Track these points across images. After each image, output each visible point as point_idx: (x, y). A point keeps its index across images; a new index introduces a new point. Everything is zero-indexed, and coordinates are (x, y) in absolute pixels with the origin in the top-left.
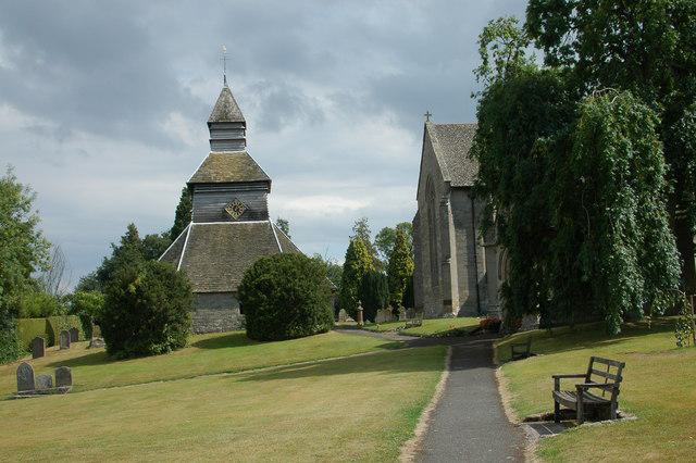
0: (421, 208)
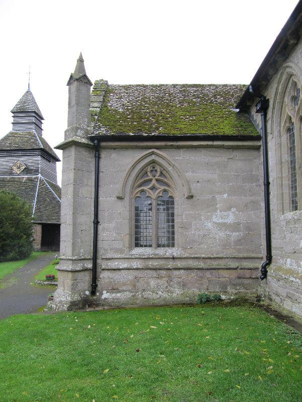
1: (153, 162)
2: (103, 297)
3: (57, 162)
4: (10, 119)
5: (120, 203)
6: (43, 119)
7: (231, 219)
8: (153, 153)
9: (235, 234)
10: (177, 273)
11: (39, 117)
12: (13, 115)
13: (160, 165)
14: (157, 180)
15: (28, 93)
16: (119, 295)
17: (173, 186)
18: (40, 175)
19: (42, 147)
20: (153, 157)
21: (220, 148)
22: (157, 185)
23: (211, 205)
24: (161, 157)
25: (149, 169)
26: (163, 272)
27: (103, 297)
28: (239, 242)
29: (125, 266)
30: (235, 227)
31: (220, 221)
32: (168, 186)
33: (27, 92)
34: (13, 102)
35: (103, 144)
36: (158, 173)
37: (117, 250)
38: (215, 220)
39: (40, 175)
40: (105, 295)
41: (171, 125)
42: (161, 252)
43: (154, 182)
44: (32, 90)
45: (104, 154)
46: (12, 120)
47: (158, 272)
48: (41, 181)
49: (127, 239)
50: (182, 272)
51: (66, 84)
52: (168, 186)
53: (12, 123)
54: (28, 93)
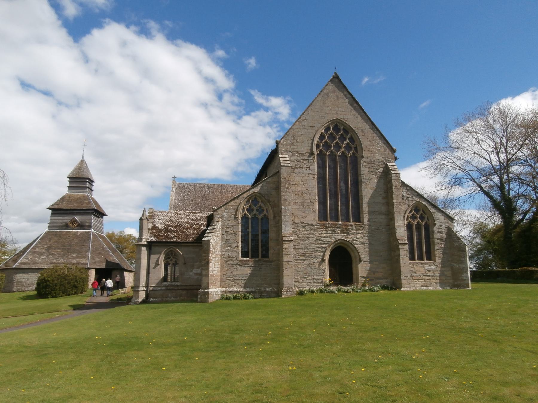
1: (171, 251)
2: (151, 300)
3: (104, 217)
4: (66, 182)
6: (93, 182)
8: (171, 248)
12: (69, 179)
14: (173, 257)
15: (83, 162)
16: (157, 299)
18: (92, 230)
19: (96, 208)
20: (172, 249)
22: (173, 259)
23: (193, 267)
24: (173, 248)
25: (170, 253)
27: (151, 300)
29: (159, 289)
31: (196, 272)
33: (82, 161)
34: (69, 170)
35: (153, 244)
36: (173, 255)
37: (232, 219)
38: (194, 272)
39: (92, 230)
40: (152, 299)
43: (172, 258)
45: (153, 248)
46: (68, 184)
48: (94, 235)
50: (181, 291)
52: (177, 259)
53: (68, 186)
54: (83, 162)
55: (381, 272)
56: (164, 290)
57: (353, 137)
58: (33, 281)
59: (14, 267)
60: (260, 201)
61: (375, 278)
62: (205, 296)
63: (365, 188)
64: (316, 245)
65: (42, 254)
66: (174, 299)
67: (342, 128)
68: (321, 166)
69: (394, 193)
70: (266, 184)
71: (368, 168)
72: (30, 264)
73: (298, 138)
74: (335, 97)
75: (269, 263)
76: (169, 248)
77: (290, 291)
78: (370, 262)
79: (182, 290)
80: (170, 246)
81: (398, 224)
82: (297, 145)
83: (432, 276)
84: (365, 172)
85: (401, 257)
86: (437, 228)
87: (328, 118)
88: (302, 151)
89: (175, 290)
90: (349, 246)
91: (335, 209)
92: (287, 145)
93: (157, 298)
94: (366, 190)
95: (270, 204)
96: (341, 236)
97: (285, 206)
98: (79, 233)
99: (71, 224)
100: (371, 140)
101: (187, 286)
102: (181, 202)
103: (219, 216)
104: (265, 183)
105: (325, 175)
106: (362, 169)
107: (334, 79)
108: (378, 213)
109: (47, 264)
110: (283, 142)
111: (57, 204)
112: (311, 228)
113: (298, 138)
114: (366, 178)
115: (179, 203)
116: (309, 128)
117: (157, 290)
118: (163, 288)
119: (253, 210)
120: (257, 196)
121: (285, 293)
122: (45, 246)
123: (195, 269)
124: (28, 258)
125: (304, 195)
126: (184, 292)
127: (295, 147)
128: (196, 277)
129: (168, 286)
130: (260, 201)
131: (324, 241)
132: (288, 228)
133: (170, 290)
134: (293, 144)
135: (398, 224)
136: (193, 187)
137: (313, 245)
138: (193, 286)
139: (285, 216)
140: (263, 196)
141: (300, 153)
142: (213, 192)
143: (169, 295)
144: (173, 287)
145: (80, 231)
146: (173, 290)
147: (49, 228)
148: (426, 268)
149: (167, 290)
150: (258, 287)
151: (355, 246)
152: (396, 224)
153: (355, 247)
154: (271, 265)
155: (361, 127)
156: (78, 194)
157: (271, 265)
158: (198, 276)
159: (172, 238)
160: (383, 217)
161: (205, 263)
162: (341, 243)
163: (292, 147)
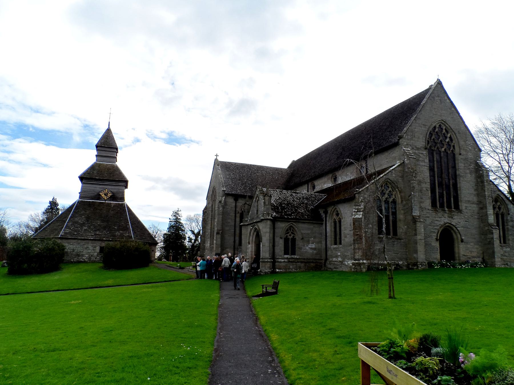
0: (208, 203)
1: (291, 226)
5: (281, 240)
7: (313, 246)
9: (315, 251)
10: (298, 263)
11: (115, 149)
13: (294, 228)
15: (109, 131)
17: (296, 234)
21: (12, 186)
23: (308, 242)
26: (294, 263)
28: (316, 254)
30: (315, 249)
31: (311, 247)
32: (295, 234)
38: (309, 246)
40: (277, 270)
41: (409, 176)
42: (293, 256)
43: (290, 233)
44: (111, 127)
47: (293, 263)
49: (283, 252)
50: (300, 263)
51: (225, 158)
52: (295, 234)
54: (109, 131)
55: (476, 252)
56: (287, 262)
57: (452, 136)
58: (78, 253)
59: (59, 236)
60: (390, 186)
61: (472, 256)
62: (361, 267)
63: (462, 181)
64: (431, 227)
65: (83, 225)
66: (295, 270)
67: (444, 128)
68: (431, 161)
69: (486, 186)
70: (395, 172)
71: (464, 164)
72: (74, 234)
73: (416, 134)
74: (439, 101)
75: (399, 241)
76: (289, 225)
77: (424, 265)
78: (8, 266)
79: (302, 262)
80: (291, 222)
81: (489, 213)
82: (414, 140)
83: (508, 256)
84: (462, 168)
85: (495, 240)
86: (510, 218)
87: (435, 119)
88: (418, 146)
89: (296, 262)
90: (453, 229)
91: (441, 196)
92: (408, 140)
93: (281, 269)
94: (463, 182)
95: (398, 190)
96: (447, 220)
97: (414, 192)
98: (113, 205)
99: (104, 195)
100: (465, 141)
101: (304, 259)
102: (230, 180)
103: (362, 198)
104: (394, 171)
105: (434, 166)
106: (460, 164)
107: (438, 85)
108: (472, 202)
109: (92, 235)
110: (405, 137)
111: (88, 173)
112: (427, 212)
113: (416, 134)
114: (462, 172)
115: (228, 181)
116: (422, 126)
117: (281, 262)
118: (286, 260)
119: (384, 194)
120: (389, 183)
121: (420, 266)
122: (83, 217)
123: (310, 244)
124: (70, 228)
125: (422, 184)
126: (303, 265)
127: (414, 142)
128: (311, 251)
129: (290, 259)
130: (390, 186)
131: (436, 224)
132: (417, 211)
133: (292, 262)
134: (411, 139)
135: (489, 213)
136: (235, 167)
137: (429, 227)
138: (309, 259)
139: (414, 201)
140: (393, 182)
141: (417, 147)
142: (255, 173)
143: (291, 267)
144: (294, 260)
145: (113, 203)
146: (294, 262)
147: (80, 197)
148: (504, 250)
149: (289, 262)
150: (393, 260)
151: (458, 229)
152: (488, 212)
153: (458, 230)
154: (401, 242)
155: (458, 129)
156: (107, 164)
157: (401, 242)
158: (313, 251)
159: (290, 215)
160: (475, 206)
161: (358, 238)
162: (448, 226)
163: (412, 141)
